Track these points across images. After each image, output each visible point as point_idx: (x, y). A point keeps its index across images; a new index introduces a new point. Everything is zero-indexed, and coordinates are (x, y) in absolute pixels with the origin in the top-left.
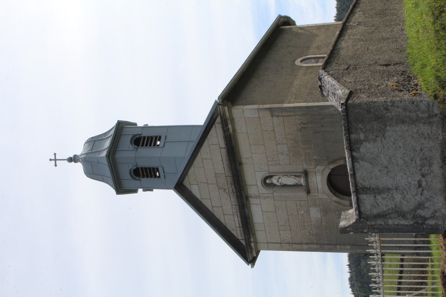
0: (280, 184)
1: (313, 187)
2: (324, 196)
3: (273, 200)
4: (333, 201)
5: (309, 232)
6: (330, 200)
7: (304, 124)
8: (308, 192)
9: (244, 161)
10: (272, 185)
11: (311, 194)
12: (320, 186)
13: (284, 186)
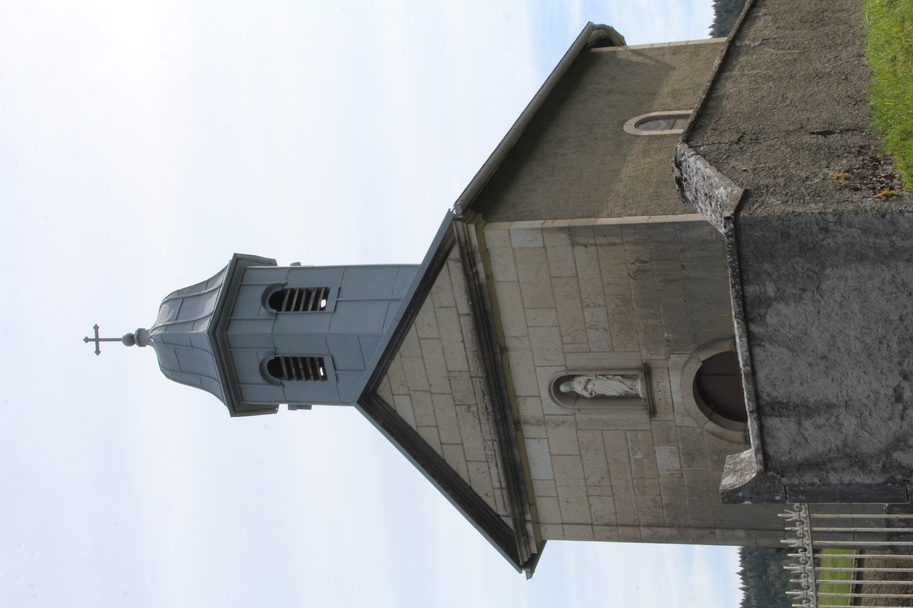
1: (663, 400)
3: (574, 430)
8: (653, 412)
9: (511, 343)
10: (573, 397)
12: (677, 399)
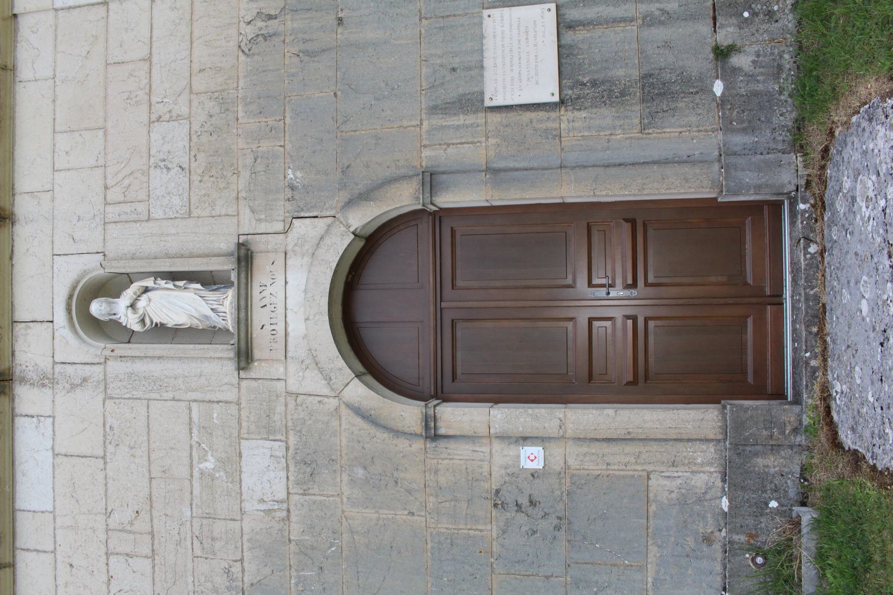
0: (143, 321)
1: (268, 328)
2: (313, 383)
3: (101, 397)
4: (349, 406)
5: (227, 572)
6: (334, 402)
7: (270, 17)
8: (245, 356)
11: (258, 369)
12: (297, 327)
13: (161, 332)
